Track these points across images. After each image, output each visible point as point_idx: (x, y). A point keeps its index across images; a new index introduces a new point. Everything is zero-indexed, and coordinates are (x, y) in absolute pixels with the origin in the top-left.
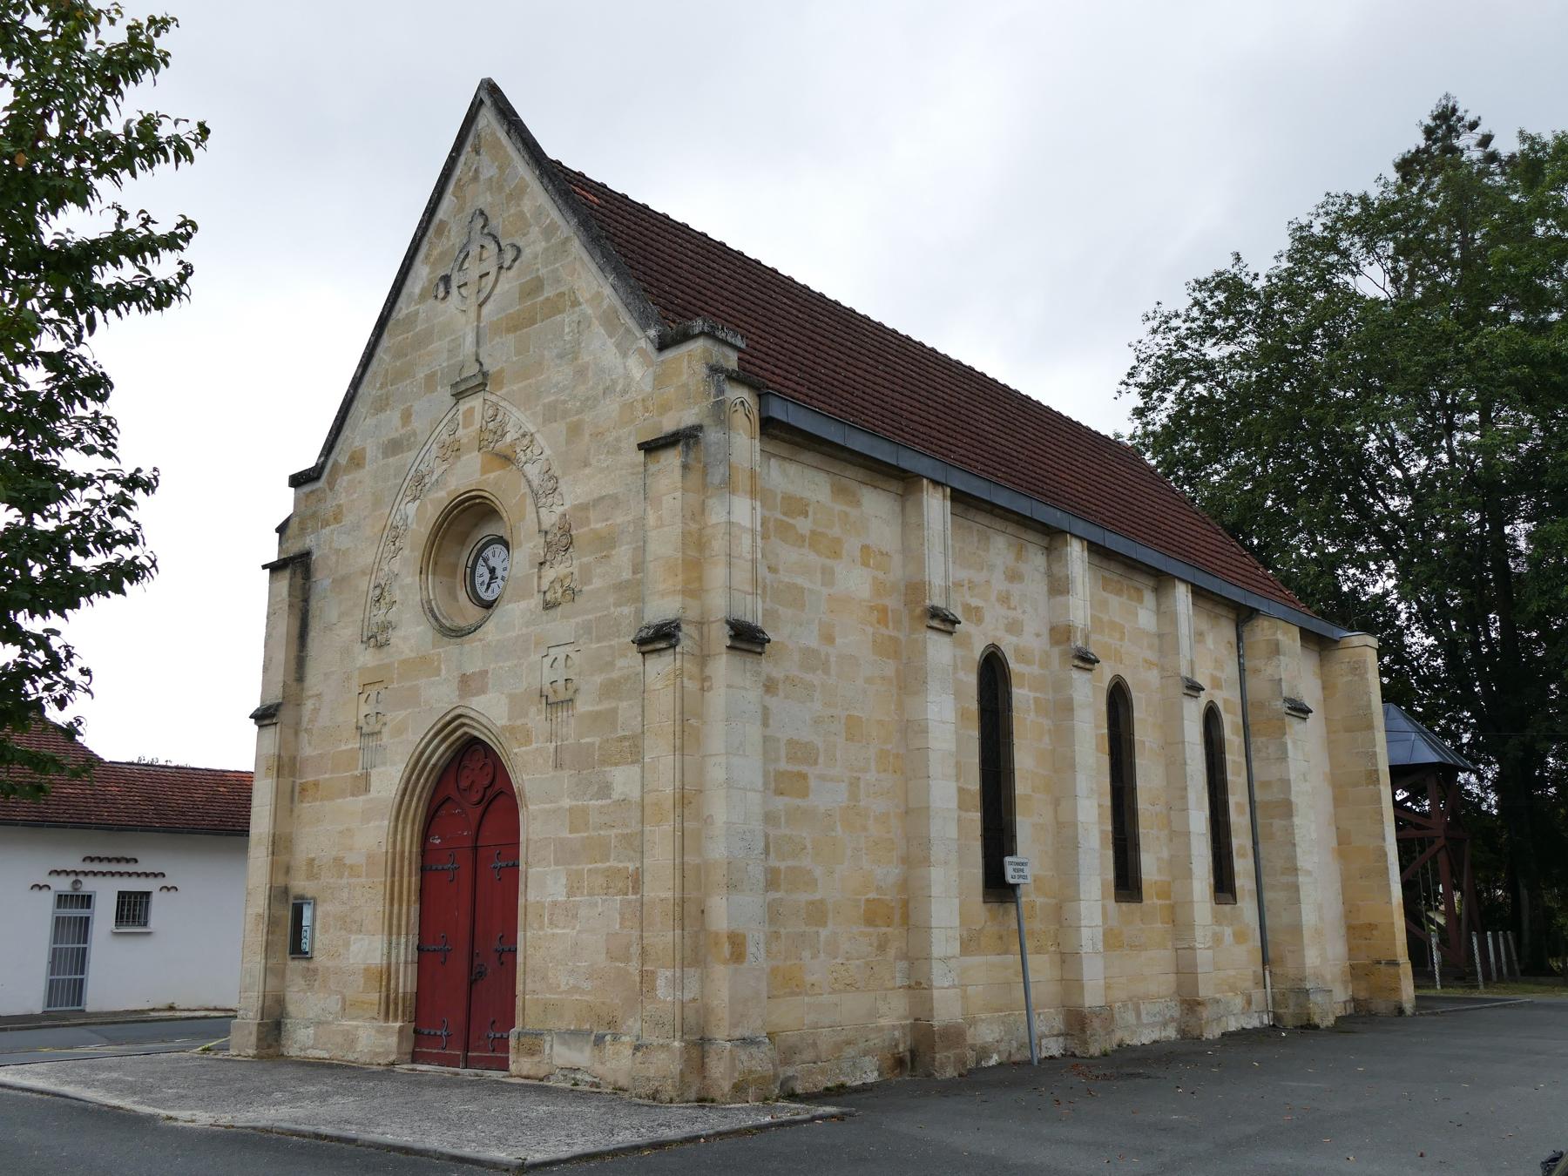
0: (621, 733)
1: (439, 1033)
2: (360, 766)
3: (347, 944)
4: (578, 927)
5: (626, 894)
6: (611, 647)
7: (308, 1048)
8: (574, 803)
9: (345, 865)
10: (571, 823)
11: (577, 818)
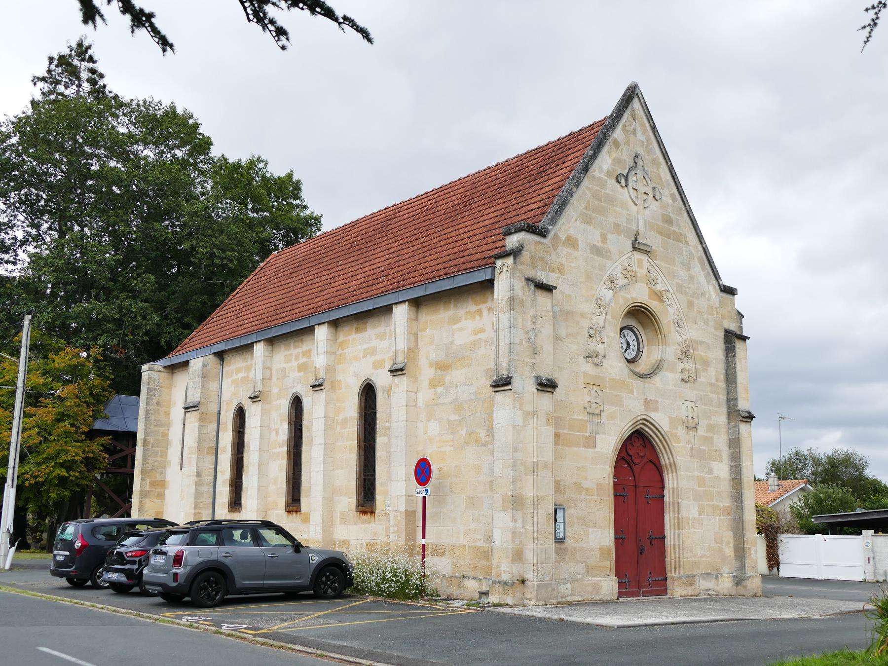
0: (715, 448)
1: (624, 581)
2: (588, 431)
3: (587, 534)
4: (704, 529)
5: (720, 516)
6: (710, 410)
7: (568, 596)
8: (699, 474)
9: (582, 487)
10: (699, 483)
11: (701, 481)
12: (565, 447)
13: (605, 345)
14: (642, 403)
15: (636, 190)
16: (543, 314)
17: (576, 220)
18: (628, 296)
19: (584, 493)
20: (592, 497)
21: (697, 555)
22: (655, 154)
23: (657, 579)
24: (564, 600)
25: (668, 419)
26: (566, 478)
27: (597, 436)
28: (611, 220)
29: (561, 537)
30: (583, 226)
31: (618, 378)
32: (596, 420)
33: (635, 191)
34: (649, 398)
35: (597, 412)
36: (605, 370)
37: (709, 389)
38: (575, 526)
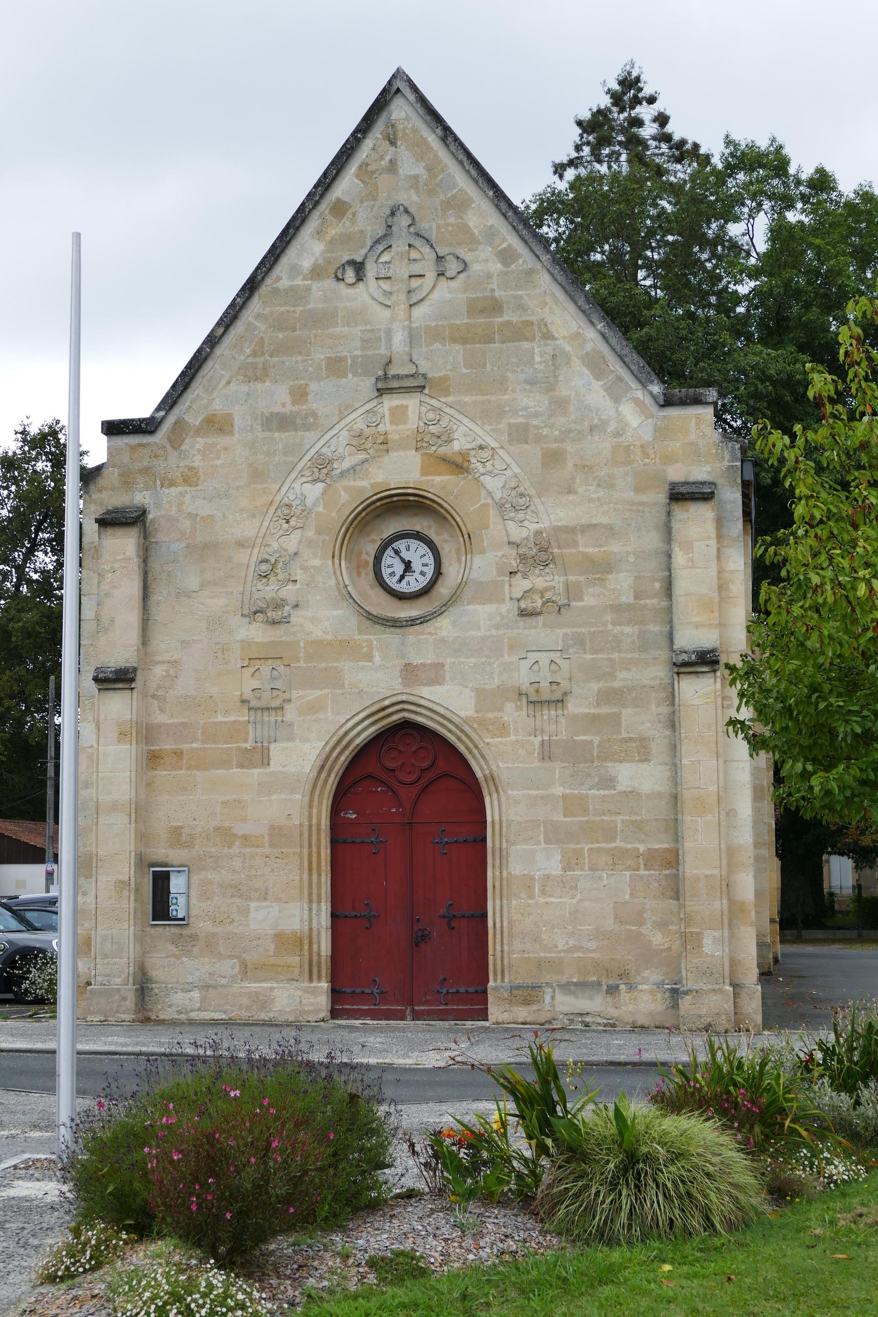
0: (624, 735)
3: (246, 912)
4: (578, 897)
7: (192, 1011)
12: (194, 772)
13: (298, 585)
14: (397, 673)
15: (389, 278)
16: (116, 565)
17: (228, 383)
18: (364, 483)
19: (237, 843)
20: (258, 850)
21: (556, 946)
22: (455, 185)
23: (462, 990)
24: (183, 1017)
25: (472, 694)
26: (196, 823)
27: (272, 746)
28: (320, 355)
29: (180, 916)
30: (245, 388)
31: (330, 637)
32: (272, 719)
33: (388, 281)
34: (417, 661)
35: (276, 703)
36: (296, 629)
37: (609, 617)
38: (216, 898)
